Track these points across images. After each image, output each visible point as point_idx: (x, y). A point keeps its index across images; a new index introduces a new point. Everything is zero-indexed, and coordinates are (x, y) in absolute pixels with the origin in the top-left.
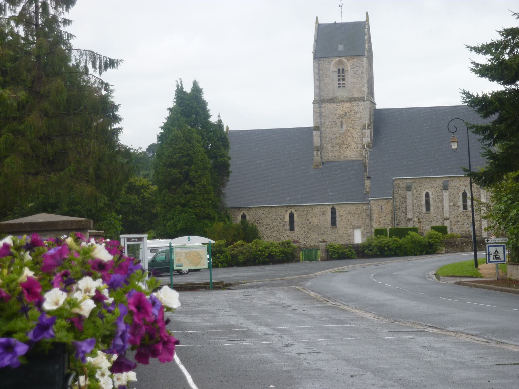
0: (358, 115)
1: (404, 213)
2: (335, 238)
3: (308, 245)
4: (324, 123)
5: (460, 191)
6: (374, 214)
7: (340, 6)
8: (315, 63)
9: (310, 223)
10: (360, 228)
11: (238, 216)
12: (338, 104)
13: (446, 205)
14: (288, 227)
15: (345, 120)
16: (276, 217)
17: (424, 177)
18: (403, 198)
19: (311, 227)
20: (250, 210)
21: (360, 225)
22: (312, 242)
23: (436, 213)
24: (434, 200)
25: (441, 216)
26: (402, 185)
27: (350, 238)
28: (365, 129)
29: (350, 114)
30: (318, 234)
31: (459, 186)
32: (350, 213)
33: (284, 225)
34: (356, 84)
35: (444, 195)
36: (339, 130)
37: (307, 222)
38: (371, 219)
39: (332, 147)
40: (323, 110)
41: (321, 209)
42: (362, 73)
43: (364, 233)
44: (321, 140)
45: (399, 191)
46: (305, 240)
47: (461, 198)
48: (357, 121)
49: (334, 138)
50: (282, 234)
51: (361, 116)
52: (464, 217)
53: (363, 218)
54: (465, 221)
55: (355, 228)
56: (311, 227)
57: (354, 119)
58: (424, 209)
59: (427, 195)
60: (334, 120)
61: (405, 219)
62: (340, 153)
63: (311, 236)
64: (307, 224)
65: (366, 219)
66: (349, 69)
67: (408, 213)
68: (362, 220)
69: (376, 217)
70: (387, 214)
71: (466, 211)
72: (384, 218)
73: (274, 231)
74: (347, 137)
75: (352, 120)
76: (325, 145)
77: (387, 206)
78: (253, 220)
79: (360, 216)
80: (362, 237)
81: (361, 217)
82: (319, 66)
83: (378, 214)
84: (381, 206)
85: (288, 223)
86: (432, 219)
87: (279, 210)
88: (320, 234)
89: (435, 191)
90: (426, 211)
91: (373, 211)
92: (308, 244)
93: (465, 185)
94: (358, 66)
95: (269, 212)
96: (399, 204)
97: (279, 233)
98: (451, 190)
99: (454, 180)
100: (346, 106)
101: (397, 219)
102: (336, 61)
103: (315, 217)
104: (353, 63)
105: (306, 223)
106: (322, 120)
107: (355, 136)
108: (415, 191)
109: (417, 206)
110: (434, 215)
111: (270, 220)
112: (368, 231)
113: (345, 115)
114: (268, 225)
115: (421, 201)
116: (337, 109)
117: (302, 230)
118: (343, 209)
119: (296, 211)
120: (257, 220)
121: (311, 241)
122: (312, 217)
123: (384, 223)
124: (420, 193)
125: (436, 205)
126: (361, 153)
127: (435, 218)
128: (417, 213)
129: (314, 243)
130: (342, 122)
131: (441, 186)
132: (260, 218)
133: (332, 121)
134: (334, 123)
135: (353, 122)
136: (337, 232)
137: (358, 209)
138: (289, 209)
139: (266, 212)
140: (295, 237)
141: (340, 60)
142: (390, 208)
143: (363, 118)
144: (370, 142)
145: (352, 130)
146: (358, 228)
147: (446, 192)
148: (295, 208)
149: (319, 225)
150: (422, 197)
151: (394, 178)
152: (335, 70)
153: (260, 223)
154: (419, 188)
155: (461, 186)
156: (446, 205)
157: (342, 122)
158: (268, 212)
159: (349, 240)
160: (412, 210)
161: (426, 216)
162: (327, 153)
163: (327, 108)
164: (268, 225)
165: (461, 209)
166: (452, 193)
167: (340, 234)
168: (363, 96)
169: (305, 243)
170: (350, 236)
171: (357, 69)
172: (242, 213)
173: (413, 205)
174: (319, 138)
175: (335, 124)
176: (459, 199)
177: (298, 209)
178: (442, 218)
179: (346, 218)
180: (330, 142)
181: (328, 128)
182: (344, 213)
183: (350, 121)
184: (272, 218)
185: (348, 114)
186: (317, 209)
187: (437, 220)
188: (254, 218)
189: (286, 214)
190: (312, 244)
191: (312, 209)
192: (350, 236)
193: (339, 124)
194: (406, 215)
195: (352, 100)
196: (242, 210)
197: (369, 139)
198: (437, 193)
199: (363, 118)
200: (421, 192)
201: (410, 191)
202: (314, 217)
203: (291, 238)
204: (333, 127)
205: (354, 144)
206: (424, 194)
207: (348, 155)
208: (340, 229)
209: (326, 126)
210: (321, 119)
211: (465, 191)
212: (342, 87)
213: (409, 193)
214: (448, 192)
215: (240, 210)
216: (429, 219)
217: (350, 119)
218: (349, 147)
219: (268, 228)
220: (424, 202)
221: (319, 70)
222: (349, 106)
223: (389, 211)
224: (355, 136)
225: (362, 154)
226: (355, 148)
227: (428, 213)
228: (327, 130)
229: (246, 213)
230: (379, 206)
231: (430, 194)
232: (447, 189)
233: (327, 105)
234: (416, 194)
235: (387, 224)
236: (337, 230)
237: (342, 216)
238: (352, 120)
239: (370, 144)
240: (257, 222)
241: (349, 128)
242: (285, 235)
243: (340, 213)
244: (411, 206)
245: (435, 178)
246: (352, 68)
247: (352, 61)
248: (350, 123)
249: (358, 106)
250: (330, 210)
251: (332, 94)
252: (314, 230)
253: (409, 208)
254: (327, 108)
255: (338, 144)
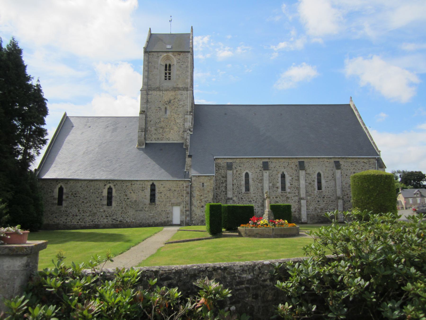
0: (181, 103)
1: (224, 192)
2: (153, 216)
3: (125, 222)
4: (150, 108)
5: (279, 173)
6: (194, 191)
7: (170, 21)
8: (145, 57)
9: (128, 199)
10: (180, 205)
11: (55, 188)
12: (164, 92)
13: (266, 185)
14: (105, 202)
15: (169, 106)
16: (94, 191)
17: (245, 157)
18: (223, 177)
19: (129, 203)
20: (68, 183)
21: (179, 203)
22: (129, 218)
23: (255, 193)
24: (253, 180)
25: (260, 196)
26: (222, 165)
27: (168, 216)
28: (187, 115)
29: (174, 102)
30: (136, 211)
31: (278, 168)
32: (170, 190)
33: (101, 200)
34: (180, 76)
35: (264, 175)
36: (163, 115)
37: (125, 197)
38: (191, 196)
39: (156, 130)
40: (149, 97)
41: (140, 184)
42: (186, 67)
43: (183, 211)
44: (146, 123)
45: (219, 170)
46: (122, 216)
47: (280, 179)
48: (180, 107)
49: (159, 122)
50: (99, 209)
51: (184, 103)
52: (282, 198)
53: (182, 196)
54: (284, 202)
55: (173, 205)
56: (129, 203)
57: (177, 106)
58: (243, 189)
59: (247, 175)
60: (159, 106)
61: (225, 198)
62: (163, 135)
63: (128, 212)
64: (125, 200)
65: (186, 196)
66: (175, 63)
67: (228, 192)
68: (182, 197)
69: (197, 194)
70: (208, 191)
71: (285, 193)
72: (205, 196)
73: (90, 206)
74: (170, 122)
75: (175, 107)
76: (149, 128)
77: (209, 183)
78: (70, 194)
79: (179, 193)
80: (181, 215)
81: (181, 195)
82: (149, 59)
83: (199, 191)
84: (203, 184)
85: (106, 198)
86: (252, 198)
87: (97, 184)
88: (138, 211)
89: (255, 172)
90: (246, 191)
91: (194, 189)
92: (125, 220)
93: (284, 167)
94: (183, 60)
95: (87, 186)
96: (219, 183)
97: (96, 208)
98: (271, 171)
99: (273, 161)
100: (171, 95)
101: (217, 198)
102: (164, 56)
103: (134, 193)
104: (179, 58)
105: (124, 199)
106: (148, 106)
107: (177, 121)
108: (235, 171)
109: (236, 185)
110: (254, 195)
111: (88, 194)
112: (187, 209)
113: (170, 102)
114: (85, 198)
115: (240, 180)
116: (162, 97)
117: (119, 205)
118: (163, 186)
119: (115, 185)
120: (74, 193)
121: (128, 217)
122: (131, 193)
123: (205, 201)
124: (240, 173)
125: (255, 185)
126: (183, 136)
127: (255, 198)
128: (237, 193)
129: (131, 219)
130: (166, 108)
131: (260, 167)
132: (78, 192)
133: (157, 107)
134: (159, 108)
135: (176, 108)
136: (155, 209)
137: (178, 186)
138: (107, 184)
139: (84, 185)
140: (112, 212)
141: (167, 55)
142: (212, 186)
143: (185, 105)
144: (191, 127)
145: (176, 115)
146: (177, 205)
147: (266, 173)
148: (114, 183)
149: (138, 201)
150: (242, 177)
151: (215, 157)
152: (163, 64)
153: (77, 197)
154: (239, 168)
155: (280, 167)
156: (266, 185)
157: (166, 108)
158: (86, 186)
159: (168, 217)
160: (232, 189)
161: (245, 196)
162: (151, 135)
163: (154, 95)
164: (85, 198)
165: (280, 190)
166: (272, 174)
167: (158, 211)
168: (186, 87)
169: (122, 219)
170: (168, 214)
171: (182, 64)
172: (59, 186)
173: (233, 185)
174: (144, 121)
175: (159, 110)
176: (278, 180)
177: (117, 184)
178: (261, 198)
179: (165, 195)
180: (154, 125)
181: (153, 112)
182: (164, 189)
183: (173, 107)
184: (90, 192)
185: (172, 101)
186: (136, 184)
187: (256, 200)
188: (71, 191)
189: (105, 189)
190: (129, 221)
191: (132, 184)
192: (168, 214)
193: (163, 110)
194: (226, 194)
195: (176, 89)
196: (59, 183)
197: (191, 124)
198: (257, 174)
199: (185, 105)
200: (241, 172)
201: (231, 170)
202: (132, 193)
203: (108, 213)
204: (157, 112)
205: (176, 128)
206: (244, 174)
207: (170, 138)
208: (159, 206)
209: (152, 111)
210: (147, 104)
211: (283, 172)
212: (168, 79)
213: (230, 172)
214: (268, 173)
215: (58, 183)
216: (248, 199)
217: (174, 106)
218: (172, 131)
219: (85, 202)
220: (243, 182)
221: (149, 62)
222: (174, 94)
223: (210, 189)
224: (177, 121)
225: (183, 138)
226: (177, 132)
227: (247, 193)
228: (152, 115)
229: (63, 186)
230: (200, 184)
231: (250, 174)
232: (268, 170)
233: (154, 93)
234: (236, 174)
235: (208, 202)
236: (155, 206)
237: (162, 192)
238: (175, 107)
239: (191, 128)
240: (74, 196)
241: (172, 114)
242: (101, 210)
243: (160, 189)
244: (232, 186)
245: (255, 158)
246: (178, 63)
247: (179, 57)
248: (173, 110)
249: (182, 94)
250: (150, 186)
251: (158, 83)
252: (132, 207)
253: (229, 187)
254: (154, 95)
255: (161, 128)
